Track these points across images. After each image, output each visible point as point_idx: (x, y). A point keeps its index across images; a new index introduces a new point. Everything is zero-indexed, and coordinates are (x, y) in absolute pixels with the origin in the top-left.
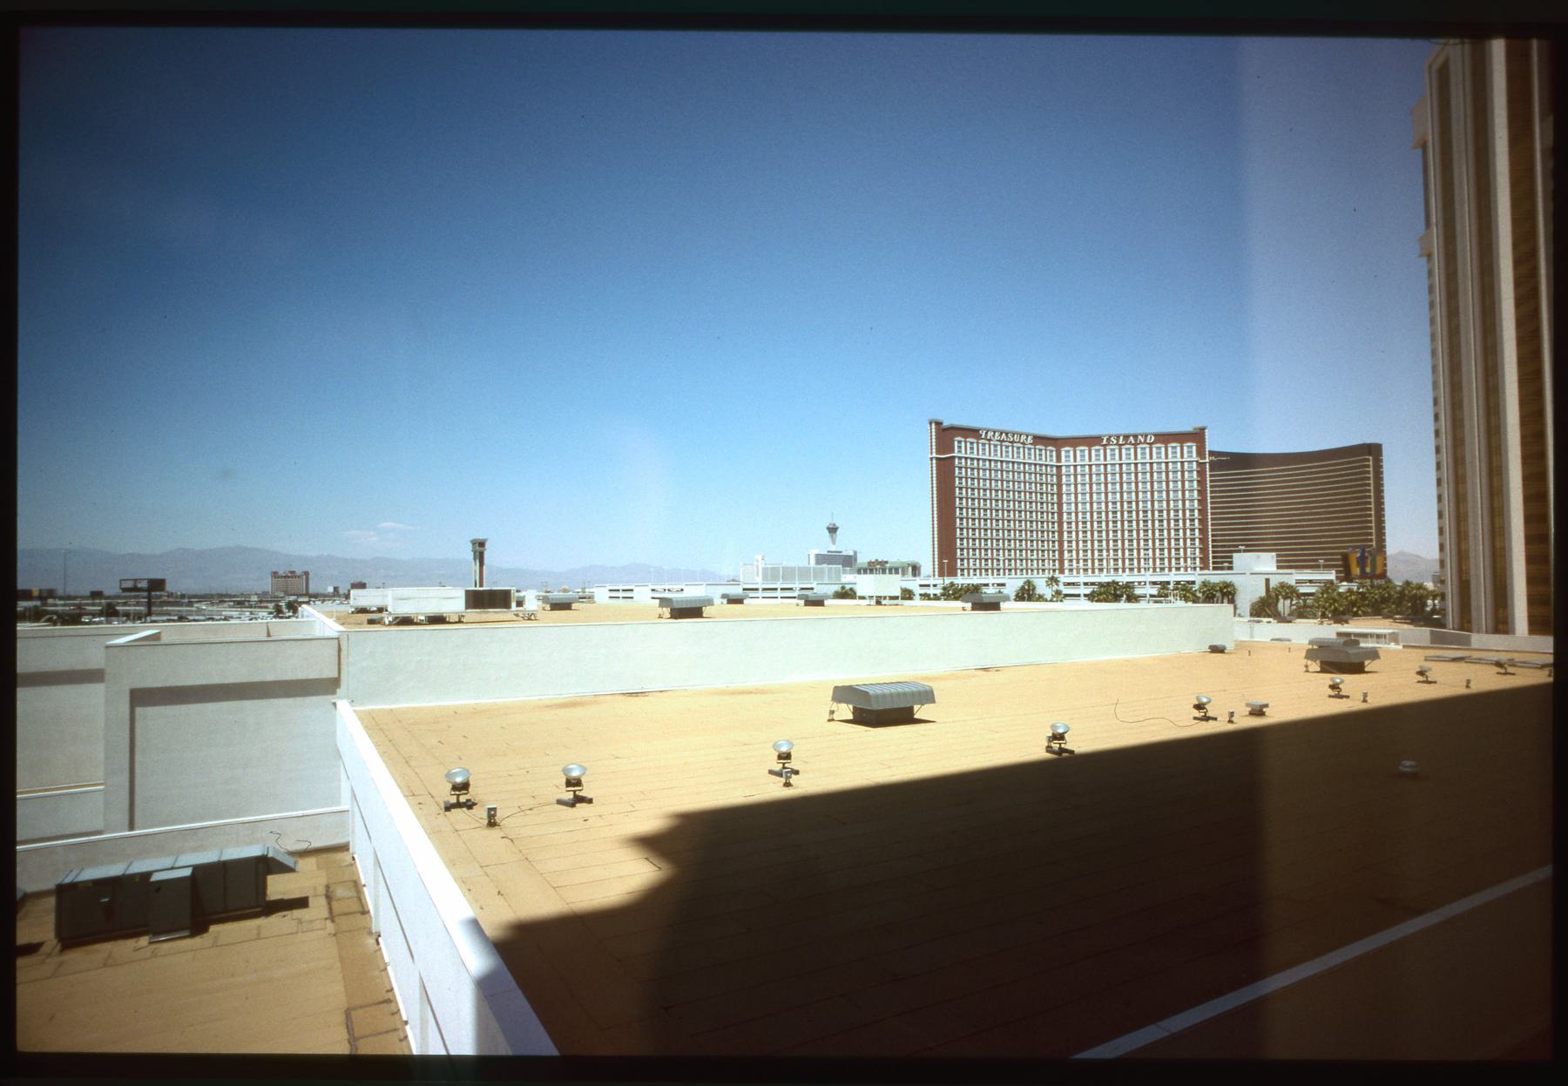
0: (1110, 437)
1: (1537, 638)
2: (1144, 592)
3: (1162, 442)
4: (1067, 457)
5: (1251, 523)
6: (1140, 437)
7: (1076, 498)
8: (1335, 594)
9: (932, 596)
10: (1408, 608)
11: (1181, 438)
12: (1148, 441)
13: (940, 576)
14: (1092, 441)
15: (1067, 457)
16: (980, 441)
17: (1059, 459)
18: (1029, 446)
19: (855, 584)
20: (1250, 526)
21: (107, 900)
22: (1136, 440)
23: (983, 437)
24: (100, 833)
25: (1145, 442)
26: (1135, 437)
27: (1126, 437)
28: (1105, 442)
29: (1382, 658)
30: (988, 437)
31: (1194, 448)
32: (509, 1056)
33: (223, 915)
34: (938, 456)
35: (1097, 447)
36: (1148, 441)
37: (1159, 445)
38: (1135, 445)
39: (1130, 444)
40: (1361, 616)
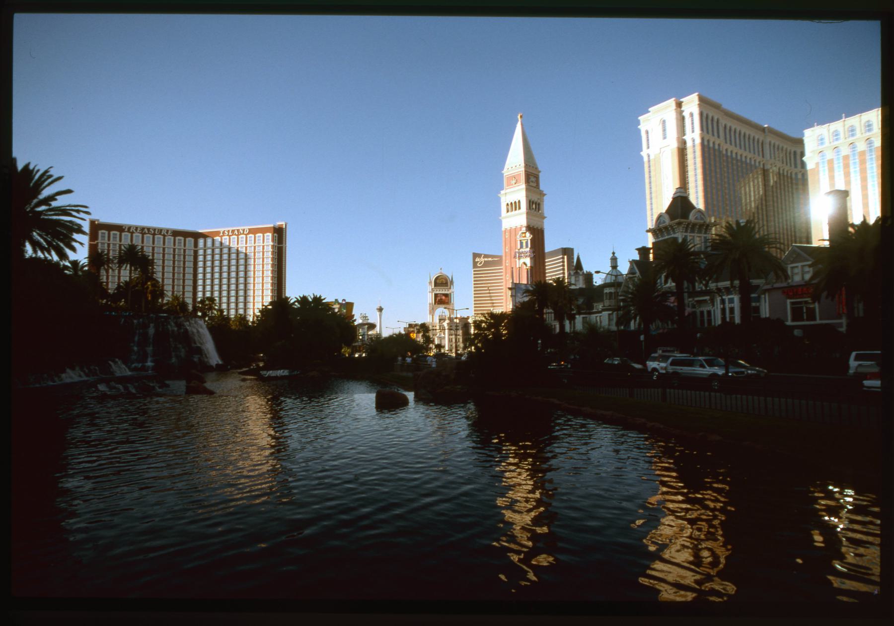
3: (252, 233)
8: (274, 256)
19: (821, 135)
20: (492, 285)
21: (708, 454)
22: (238, 233)
23: (126, 230)
25: (243, 234)
28: (221, 234)
29: (472, 252)
30: (131, 231)
36: (245, 233)
37: (251, 235)
38: (238, 235)
39: (235, 235)
40: (760, 304)
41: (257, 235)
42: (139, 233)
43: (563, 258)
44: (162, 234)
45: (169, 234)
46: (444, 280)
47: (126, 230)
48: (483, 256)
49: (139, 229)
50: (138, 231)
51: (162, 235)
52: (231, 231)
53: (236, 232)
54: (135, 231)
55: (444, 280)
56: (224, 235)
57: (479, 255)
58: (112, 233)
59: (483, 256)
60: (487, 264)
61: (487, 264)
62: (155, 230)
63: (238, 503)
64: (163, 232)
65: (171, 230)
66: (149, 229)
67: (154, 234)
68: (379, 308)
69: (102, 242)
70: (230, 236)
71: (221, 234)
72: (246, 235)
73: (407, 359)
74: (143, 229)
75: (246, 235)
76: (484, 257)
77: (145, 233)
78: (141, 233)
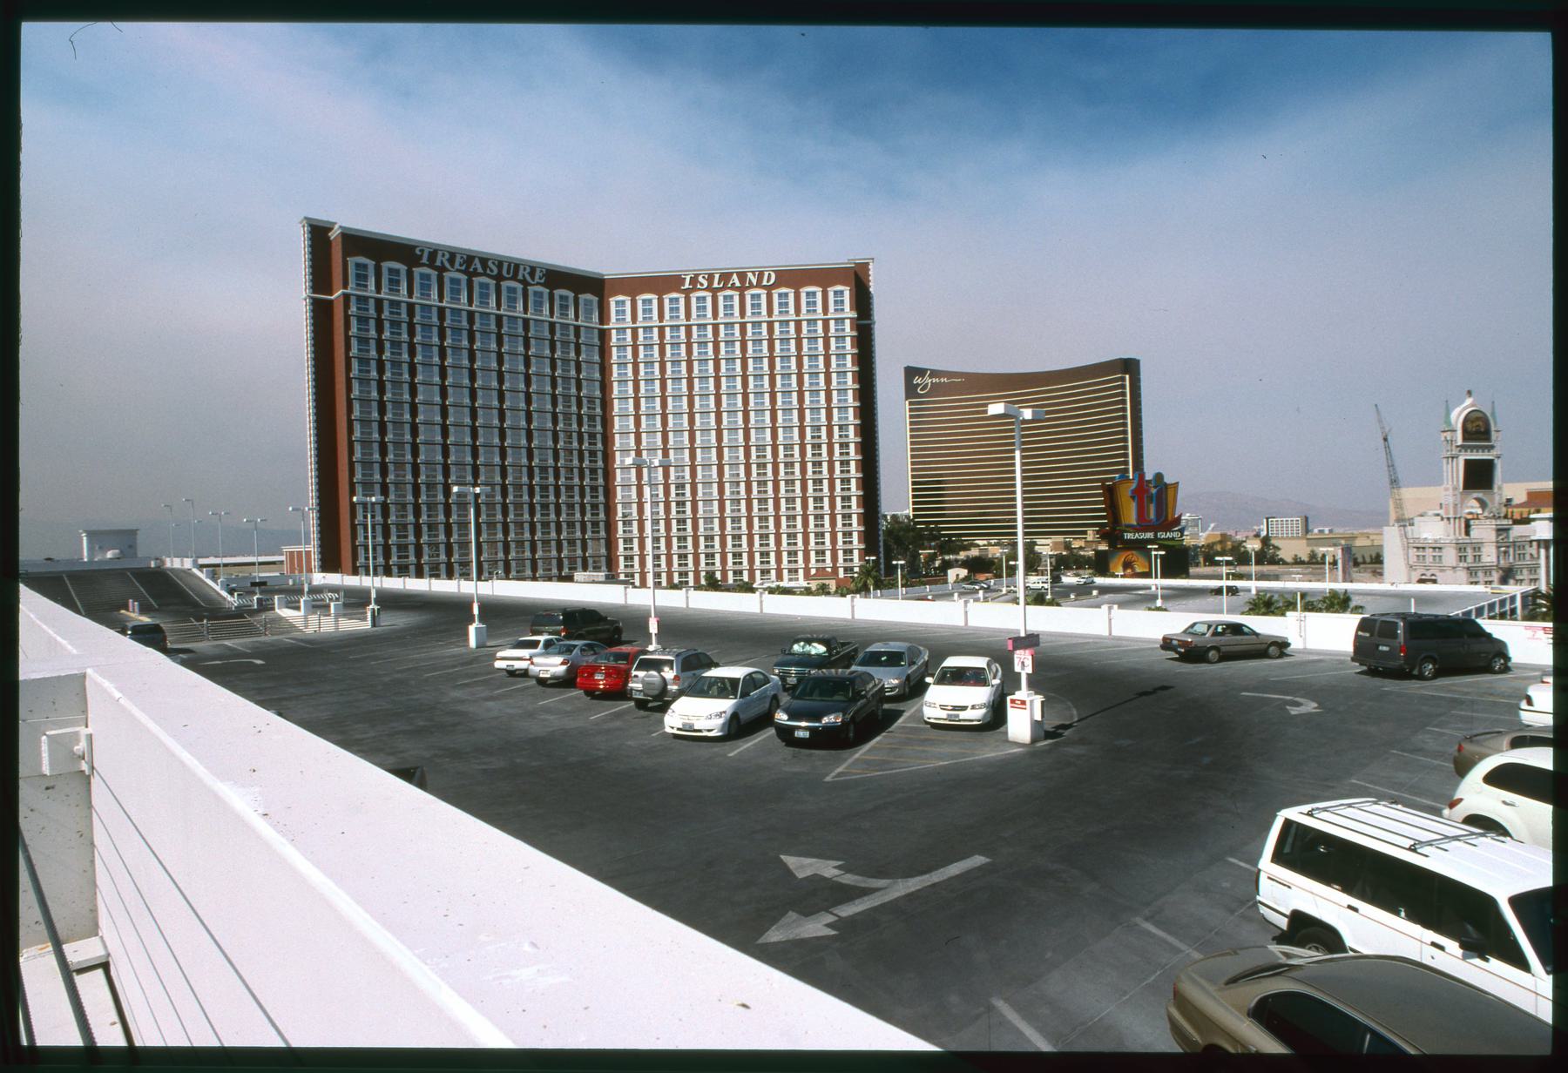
0: (697, 276)
1: (1039, 551)
4: (620, 312)
5: (1000, 431)
9: (1012, 563)
11: (824, 277)
12: (765, 283)
13: (1086, 534)
14: (664, 284)
15: (620, 312)
16: (417, 271)
17: (604, 317)
18: (540, 289)
23: (424, 260)
25: (759, 285)
26: (742, 276)
27: (725, 277)
30: (438, 263)
31: (847, 294)
32: (18, 555)
35: (675, 295)
36: (765, 283)
37: (784, 290)
38: (742, 290)
39: (733, 287)
41: (640, 298)
42: (458, 270)
43: (1123, 379)
44: (520, 277)
45: (537, 279)
46: (1481, 423)
47: (424, 260)
49: (458, 260)
50: (457, 266)
51: (520, 281)
52: (717, 276)
53: (735, 280)
54: (447, 265)
55: (1481, 423)
56: (695, 289)
57: (921, 372)
58: (386, 265)
60: (936, 390)
61: (936, 390)
62: (500, 264)
63: (1429, 803)
65: (541, 266)
66: (484, 261)
67: (499, 278)
68: (1168, 480)
70: (714, 292)
72: (769, 289)
73: (966, 571)
74: (469, 258)
75: (769, 289)
76: (931, 376)
77: (476, 274)
78: (465, 272)
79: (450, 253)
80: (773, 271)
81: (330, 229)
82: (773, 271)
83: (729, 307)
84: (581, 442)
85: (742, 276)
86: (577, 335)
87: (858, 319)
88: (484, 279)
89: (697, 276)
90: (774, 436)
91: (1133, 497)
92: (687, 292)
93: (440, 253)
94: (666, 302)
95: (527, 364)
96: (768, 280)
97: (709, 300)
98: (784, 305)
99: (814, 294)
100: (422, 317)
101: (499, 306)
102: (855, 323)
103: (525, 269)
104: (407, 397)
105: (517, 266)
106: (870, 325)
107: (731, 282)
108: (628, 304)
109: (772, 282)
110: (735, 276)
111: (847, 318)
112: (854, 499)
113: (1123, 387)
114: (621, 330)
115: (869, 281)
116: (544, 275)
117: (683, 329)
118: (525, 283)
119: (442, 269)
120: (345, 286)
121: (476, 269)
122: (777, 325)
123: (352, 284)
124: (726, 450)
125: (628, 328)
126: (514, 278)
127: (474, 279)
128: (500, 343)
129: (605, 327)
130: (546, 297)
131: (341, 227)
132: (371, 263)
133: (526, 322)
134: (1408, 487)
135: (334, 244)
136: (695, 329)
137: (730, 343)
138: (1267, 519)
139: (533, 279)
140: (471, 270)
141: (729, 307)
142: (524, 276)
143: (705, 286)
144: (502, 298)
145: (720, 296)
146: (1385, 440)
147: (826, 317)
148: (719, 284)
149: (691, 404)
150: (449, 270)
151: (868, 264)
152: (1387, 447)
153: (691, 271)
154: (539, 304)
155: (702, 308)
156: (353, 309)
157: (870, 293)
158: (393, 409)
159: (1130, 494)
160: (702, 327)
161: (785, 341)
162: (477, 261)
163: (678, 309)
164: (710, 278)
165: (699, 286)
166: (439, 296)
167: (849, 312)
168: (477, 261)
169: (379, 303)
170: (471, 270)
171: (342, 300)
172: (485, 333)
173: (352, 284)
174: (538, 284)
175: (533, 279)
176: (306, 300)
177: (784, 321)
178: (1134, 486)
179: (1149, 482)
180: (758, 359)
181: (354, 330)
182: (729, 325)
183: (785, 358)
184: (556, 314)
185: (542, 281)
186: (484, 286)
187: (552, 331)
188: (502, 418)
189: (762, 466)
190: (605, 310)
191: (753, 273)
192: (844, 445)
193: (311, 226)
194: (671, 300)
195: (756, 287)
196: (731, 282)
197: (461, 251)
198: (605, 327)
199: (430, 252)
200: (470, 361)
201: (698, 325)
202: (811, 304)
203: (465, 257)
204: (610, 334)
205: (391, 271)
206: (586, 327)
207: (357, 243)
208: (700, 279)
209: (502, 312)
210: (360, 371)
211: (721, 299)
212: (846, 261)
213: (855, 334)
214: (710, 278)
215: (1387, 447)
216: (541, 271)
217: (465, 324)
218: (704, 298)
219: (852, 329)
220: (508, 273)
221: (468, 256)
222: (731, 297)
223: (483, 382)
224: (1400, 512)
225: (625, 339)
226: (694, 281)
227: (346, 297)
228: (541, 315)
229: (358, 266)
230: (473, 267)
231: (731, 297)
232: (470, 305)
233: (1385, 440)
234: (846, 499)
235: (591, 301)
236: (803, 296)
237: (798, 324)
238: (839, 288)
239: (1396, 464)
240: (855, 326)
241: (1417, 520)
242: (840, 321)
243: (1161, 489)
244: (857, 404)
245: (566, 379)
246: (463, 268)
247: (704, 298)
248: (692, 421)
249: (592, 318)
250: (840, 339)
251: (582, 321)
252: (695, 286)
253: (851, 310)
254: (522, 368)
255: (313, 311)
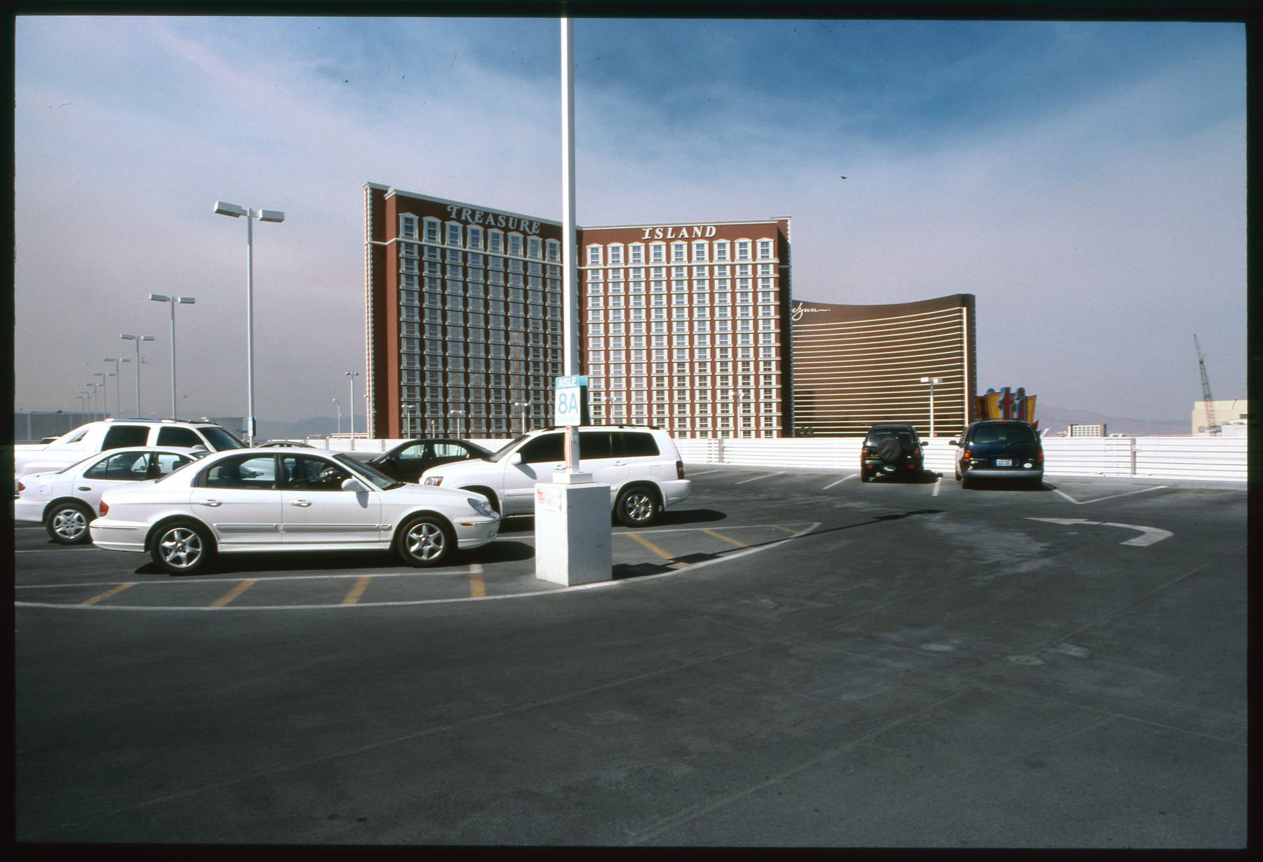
0: (655, 229)
2: (588, 465)
4: (595, 257)
6: (696, 229)
7: (690, 286)
10: (646, 504)
11: (754, 231)
12: (707, 235)
14: (628, 235)
15: (595, 257)
16: (448, 224)
23: (454, 216)
24: (713, 556)
25: (703, 237)
27: (677, 230)
28: (647, 237)
30: (463, 218)
33: (935, 655)
34: (374, 242)
35: (637, 244)
36: (707, 235)
37: (722, 241)
38: (689, 240)
39: (683, 238)
42: (477, 224)
43: (961, 311)
44: (522, 229)
45: (534, 231)
47: (454, 216)
48: (801, 304)
49: (477, 216)
51: (521, 232)
52: (670, 230)
53: (684, 232)
56: (652, 240)
58: (427, 219)
59: (801, 304)
60: (807, 318)
62: (507, 219)
64: (522, 225)
65: (537, 220)
66: (496, 216)
67: (506, 229)
69: (678, 264)
70: (668, 241)
71: (647, 237)
72: (711, 239)
74: (486, 215)
75: (711, 239)
76: (803, 307)
79: (471, 210)
80: (714, 226)
81: (386, 192)
82: (714, 226)
83: (679, 254)
84: (546, 356)
85: (690, 230)
86: (465, 260)
87: (779, 264)
88: (496, 231)
89: (655, 229)
90: (692, 355)
91: (1000, 407)
92: (647, 242)
93: (464, 211)
94: (631, 249)
95: (465, 289)
96: (710, 233)
97: (664, 248)
98: (722, 252)
99: (745, 244)
100: (473, 262)
101: (465, 245)
102: (778, 267)
103: (467, 212)
104: (439, 321)
105: (519, 221)
106: (788, 268)
107: (681, 234)
108: (601, 250)
109: (713, 234)
110: (684, 230)
111: (771, 264)
112: (774, 405)
113: (961, 317)
114: (595, 271)
115: (787, 235)
116: (482, 217)
117: (622, 271)
118: (525, 234)
119: (466, 223)
120: (397, 236)
121: (490, 222)
122: (716, 268)
123: (402, 233)
124: (612, 367)
125: (601, 269)
126: (517, 230)
127: (446, 222)
128: (465, 274)
129: (583, 268)
130: (540, 244)
131: (395, 190)
132: (416, 218)
133: (486, 258)
134: (1217, 400)
135: (388, 204)
136: (652, 270)
137: (658, 282)
138: (1072, 426)
139: (531, 230)
140: (487, 223)
141: (679, 254)
142: (524, 228)
143: (661, 237)
144: (489, 243)
145: (673, 245)
146: (1201, 363)
147: (733, 263)
148: (672, 236)
149: (628, 329)
150: (470, 224)
151: (787, 221)
152: (1203, 369)
153: (661, 225)
154: (475, 240)
155: (658, 255)
156: (403, 253)
157: (788, 243)
158: (430, 330)
159: (998, 404)
160: (658, 269)
161: (722, 281)
162: (490, 216)
163: (618, 255)
164: (665, 231)
165: (656, 237)
166: (463, 244)
167: (772, 259)
168: (490, 216)
169: (421, 248)
170: (487, 223)
171: (395, 245)
172: (454, 266)
173: (402, 233)
174: (534, 234)
175: (531, 230)
176: (367, 245)
177: (700, 266)
178: (1001, 398)
179: (1013, 395)
180: (680, 295)
181: (403, 269)
182: (679, 268)
183: (723, 294)
184: (469, 245)
185: (537, 232)
186: (496, 236)
187: (544, 271)
188: (466, 335)
189: (660, 379)
190: (583, 255)
191: (699, 227)
192: (767, 363)
193: (372, 189)
194: (634, 248)
195: (700, 238)
196: (681, 234)
197: (480, 210)
198: (583, 268)
199: (457, 209)
200: (505, 296)
201: (634, 268)
202: (743, 252)
203: (482, 213)
204: (586, 274)
205: (430, 224)
206: (513, 259)
207: (407, 203)
208: (657, 231)
209: (467, 250)
210: (407, 300)
211: (673, 248)
212: (769, 219)
213: (777, 276)
214: (665, 231)
215: (1203, 369)
216: (537, 224)
217: (460, 261)
218: (660, 247)
219: (775, 272)
220: (513, 226)
221: (485, 213)
222: (681, 246)
223: (473, 307)
224: (1212, 421)
225: (598, 278)
226: (652, 233)
227: (398, 243)
228: (498, 253)
229: (407, 220)
230: (488, 221)
231: (681, 246)
232: (465, 247)
233: (1201, 363)
234: (768, 405)
235: (518, 238)
236: (737, 245)
237: (733, 267)
238: (765, 240)
239: (1210, 383)
240: (777, 270)
241: (1224, 428)
242: (765, 266)
243: (1023, 401)
244: (778, 331)
245: (433, 295)
246: (481, 222)
247: (660, 247)
248: (607, 343)
249: (537, 256)
250: (766, 280)
251: (490, 251)
252: (653, 237)
253: (774, 257)
254: (461, 292)
255: (373, 254)
